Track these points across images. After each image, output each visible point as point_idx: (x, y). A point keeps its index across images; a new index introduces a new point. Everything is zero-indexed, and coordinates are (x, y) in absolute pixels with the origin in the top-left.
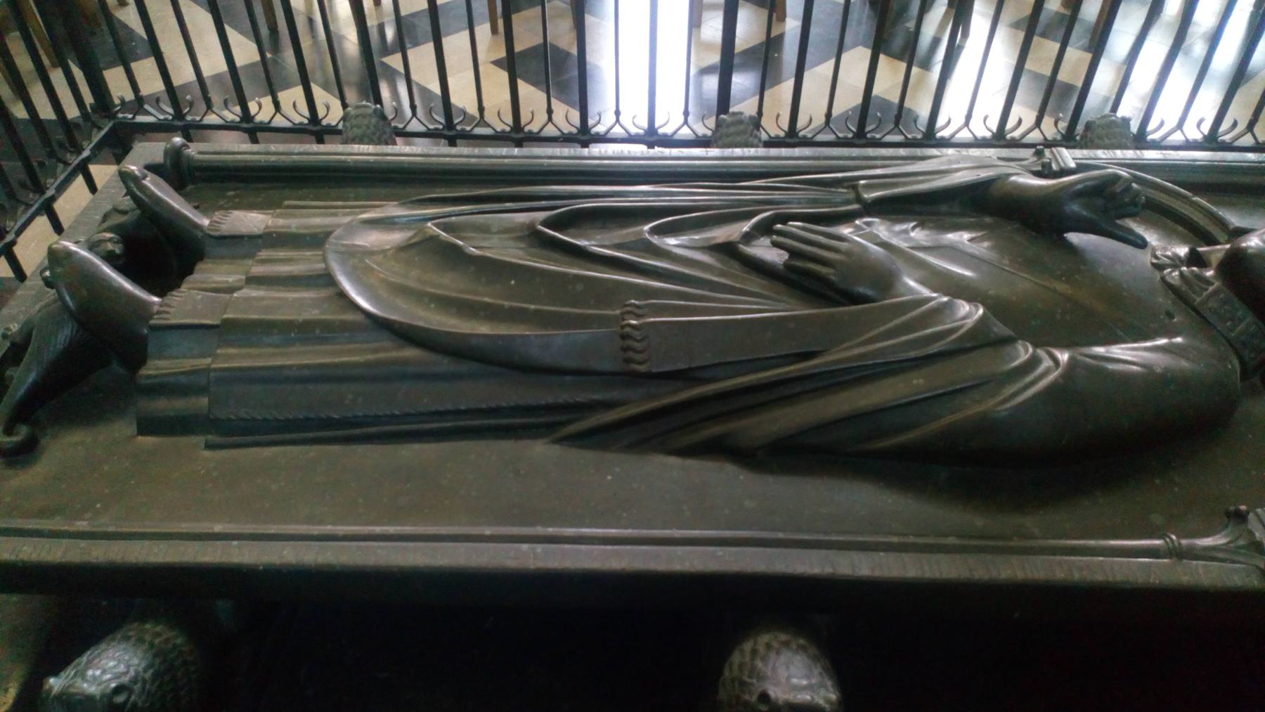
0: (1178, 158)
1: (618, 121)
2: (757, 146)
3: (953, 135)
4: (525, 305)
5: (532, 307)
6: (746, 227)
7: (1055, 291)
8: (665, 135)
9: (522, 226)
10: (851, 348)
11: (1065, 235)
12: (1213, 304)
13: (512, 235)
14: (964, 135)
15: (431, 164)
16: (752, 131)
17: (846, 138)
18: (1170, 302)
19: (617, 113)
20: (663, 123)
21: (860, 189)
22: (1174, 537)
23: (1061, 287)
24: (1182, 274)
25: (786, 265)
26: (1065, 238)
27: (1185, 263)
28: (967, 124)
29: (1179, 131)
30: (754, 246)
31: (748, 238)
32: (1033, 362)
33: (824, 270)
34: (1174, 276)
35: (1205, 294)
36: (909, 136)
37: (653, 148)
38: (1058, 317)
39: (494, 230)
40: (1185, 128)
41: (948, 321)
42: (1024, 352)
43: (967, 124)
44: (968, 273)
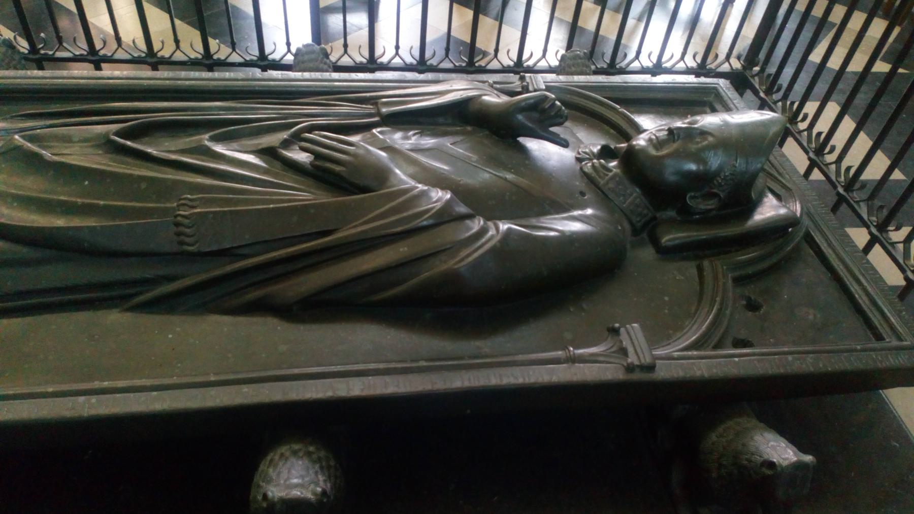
0: (639, 81)
1: (397, 53)
2: (589, 74)
3: (535, 64)
4: (96, 202)
5: (102, 203)
6: (285, 135)
7: (506, 179)
8: (274, 60)
9: (99, 136)
10: (355, 227)
11: (518, 139)
12: (611, 185)
13: (90, 144)
14: (543, 64)
15: (46, 85)
16: (323, 58)
17: (461, 66)
18: (584, 184)
19: (397, 47)
20: (619, 62)
22: (572, 349)
24: (593, 166)
25: (311, 164)
26: (518, 141)
27: (596, 157)
28: (544, 56)
30: (293, 150)
31: (286, 144)
32: (483, 231)
33: (338, 168)
35: (607, 178)
36: (599, 66)
37: (266, 71)
38: (507, 198)
39: (76, 139)
40: (640, 59)
41: (424, 204)
43: (544, 56)
44: (446, 168)
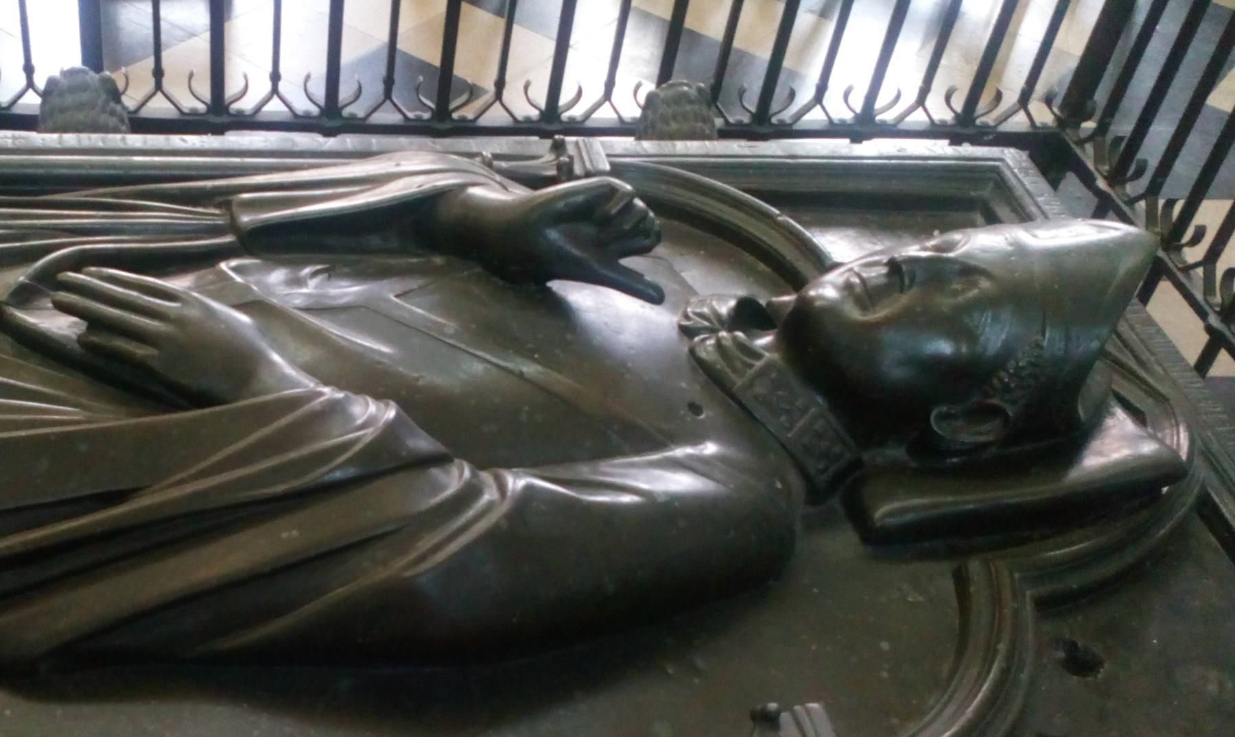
1: (275, 91)
2: (709, 138)
3: (588, 115)
7: (521, 375)
10: (181, 482)
12: (759, 389)
14: (605, 115)
16: (107, 101)
17: (419, 119)
19: (275, 77)
21: (235, 209)
23: (530, 369)
24: (719, 345)
25: (81, 340)
27: (726, 325)
28: (607, 96)
29: (920, 109)
30: (38, 309)
32: (470, 493)
33: (140, 351)
34: (707, 347)
35: (750, 372)
36: (731, 120)
40: (614, 97)
42: (456, 477)
43: (607, 96)
44: (385, 349)
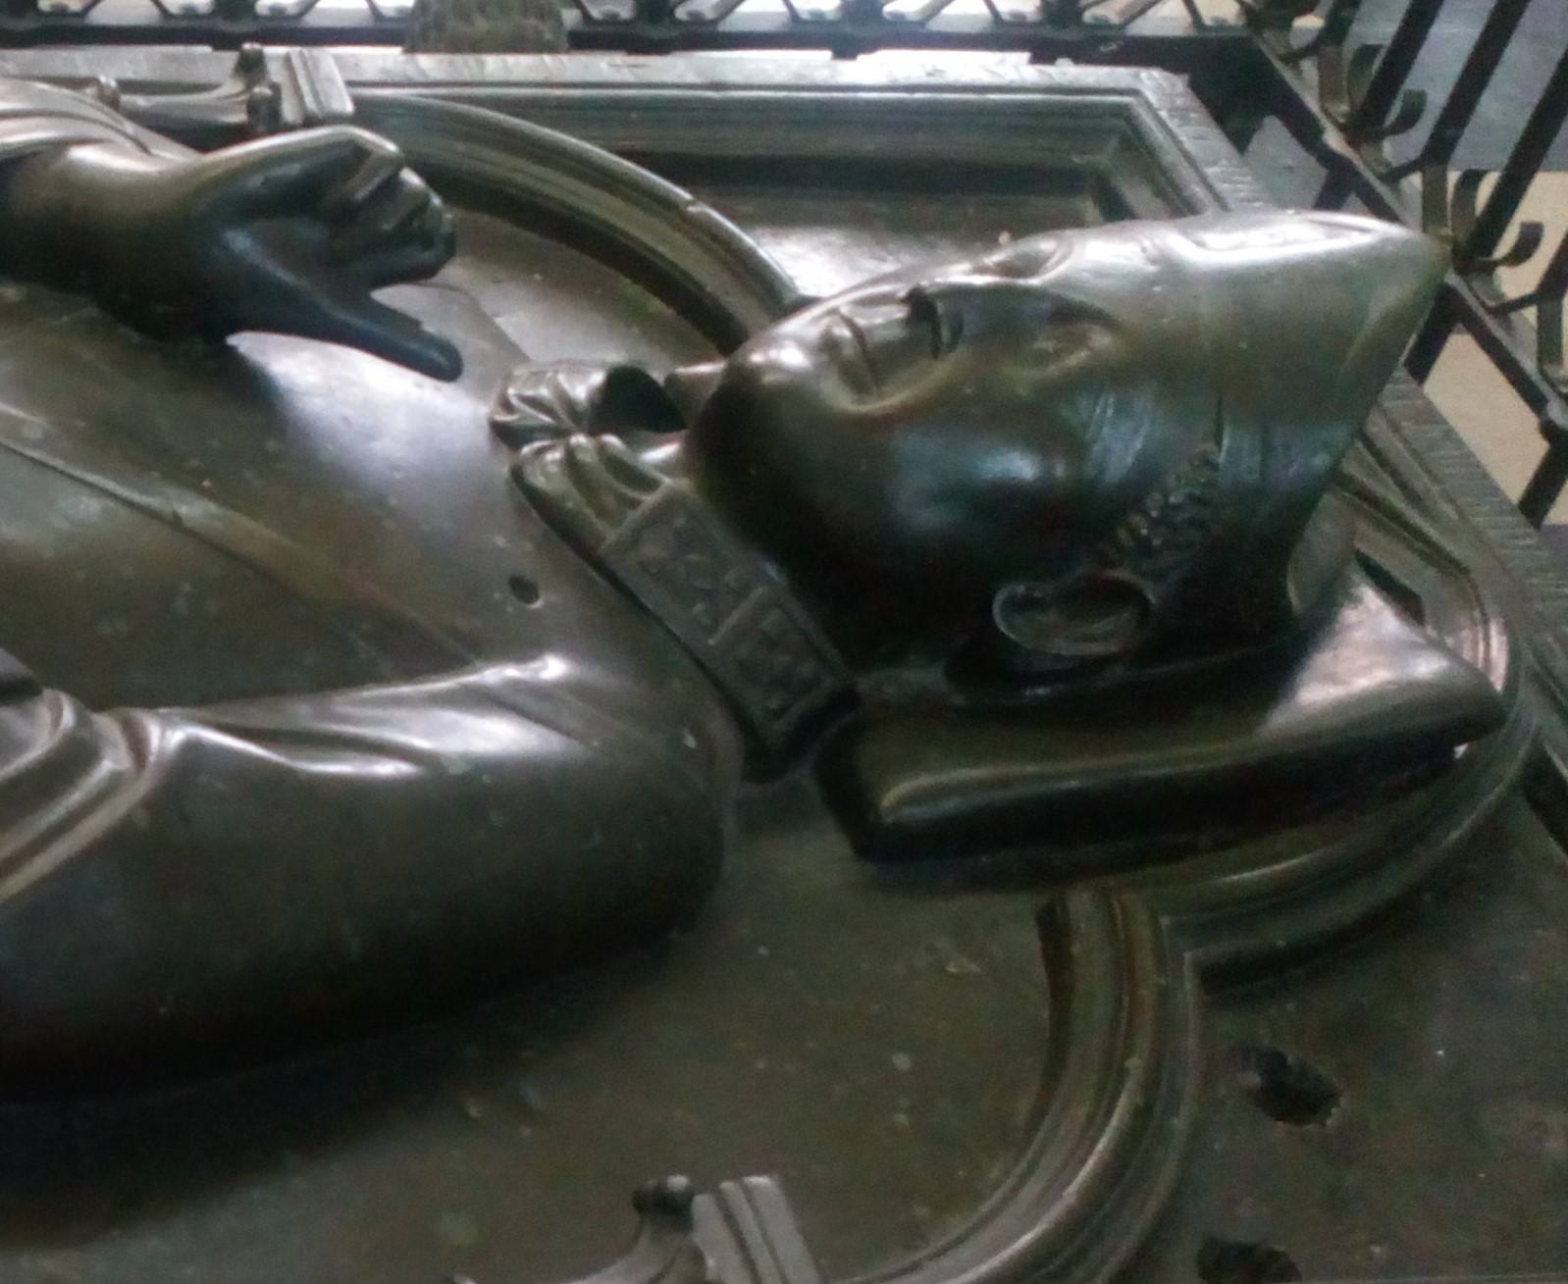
7: (175, 522)
11: (233, 340)
12: (652, 550)
23: (194, 509)
32: (73, 757)
34: (547, 465)
35: (633, 516)
36: (596, 13)
38: (181, 606)
